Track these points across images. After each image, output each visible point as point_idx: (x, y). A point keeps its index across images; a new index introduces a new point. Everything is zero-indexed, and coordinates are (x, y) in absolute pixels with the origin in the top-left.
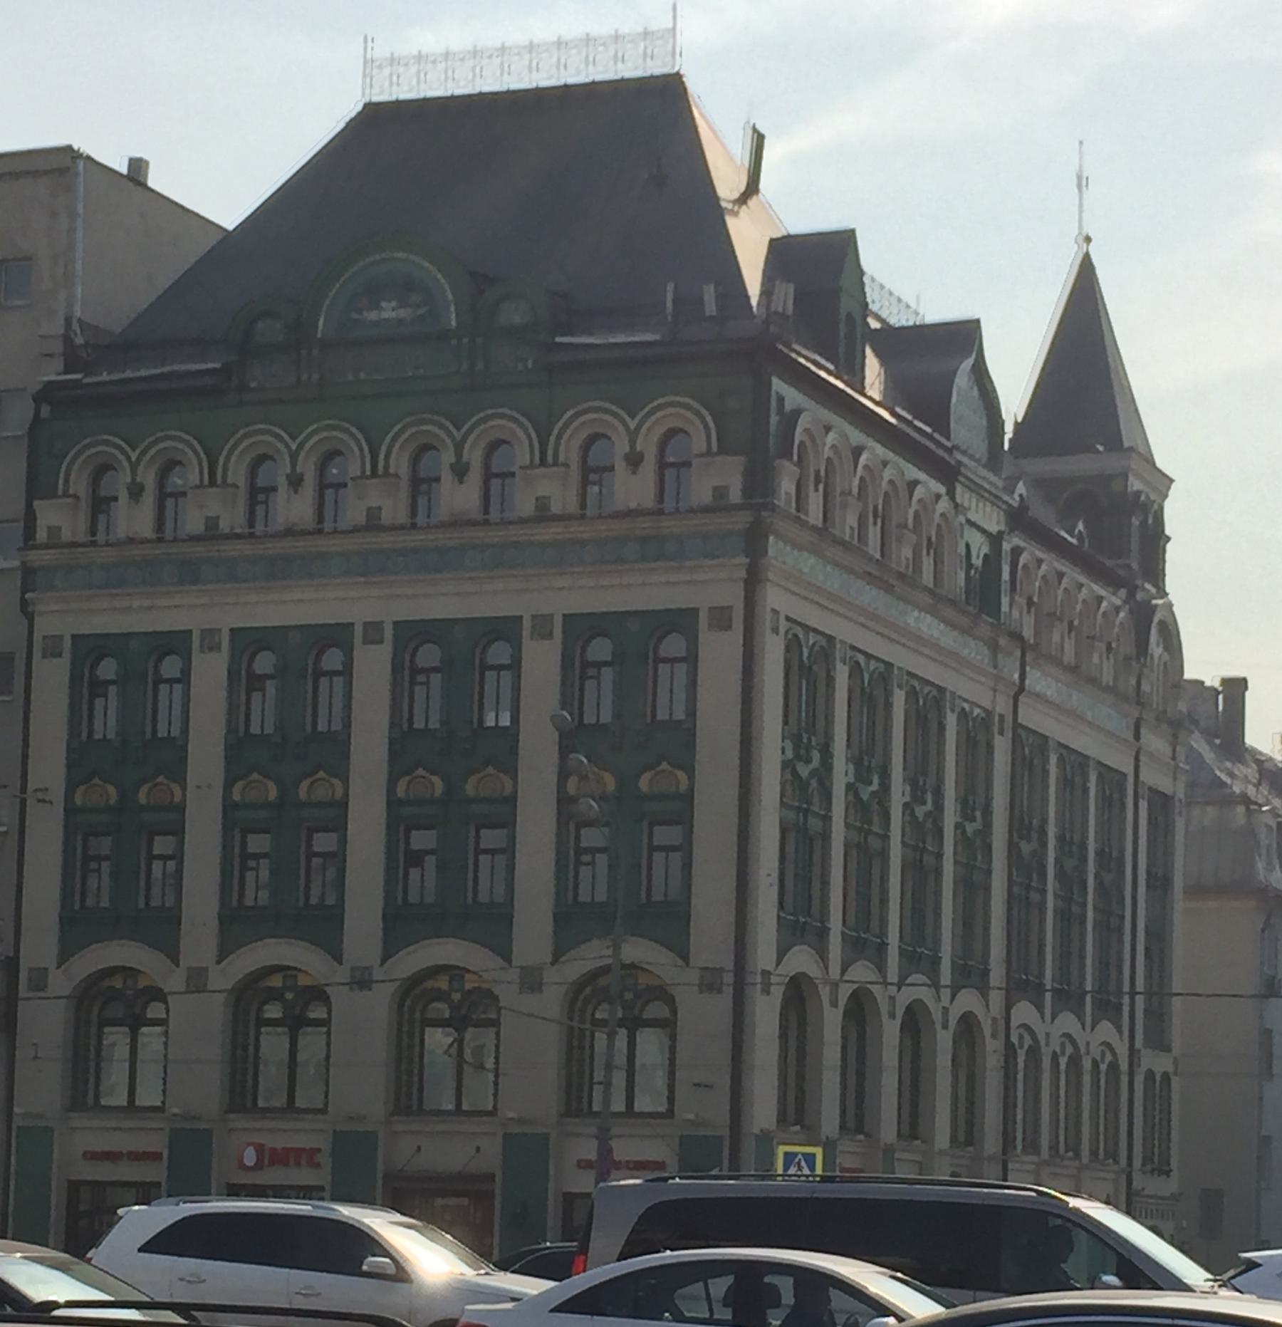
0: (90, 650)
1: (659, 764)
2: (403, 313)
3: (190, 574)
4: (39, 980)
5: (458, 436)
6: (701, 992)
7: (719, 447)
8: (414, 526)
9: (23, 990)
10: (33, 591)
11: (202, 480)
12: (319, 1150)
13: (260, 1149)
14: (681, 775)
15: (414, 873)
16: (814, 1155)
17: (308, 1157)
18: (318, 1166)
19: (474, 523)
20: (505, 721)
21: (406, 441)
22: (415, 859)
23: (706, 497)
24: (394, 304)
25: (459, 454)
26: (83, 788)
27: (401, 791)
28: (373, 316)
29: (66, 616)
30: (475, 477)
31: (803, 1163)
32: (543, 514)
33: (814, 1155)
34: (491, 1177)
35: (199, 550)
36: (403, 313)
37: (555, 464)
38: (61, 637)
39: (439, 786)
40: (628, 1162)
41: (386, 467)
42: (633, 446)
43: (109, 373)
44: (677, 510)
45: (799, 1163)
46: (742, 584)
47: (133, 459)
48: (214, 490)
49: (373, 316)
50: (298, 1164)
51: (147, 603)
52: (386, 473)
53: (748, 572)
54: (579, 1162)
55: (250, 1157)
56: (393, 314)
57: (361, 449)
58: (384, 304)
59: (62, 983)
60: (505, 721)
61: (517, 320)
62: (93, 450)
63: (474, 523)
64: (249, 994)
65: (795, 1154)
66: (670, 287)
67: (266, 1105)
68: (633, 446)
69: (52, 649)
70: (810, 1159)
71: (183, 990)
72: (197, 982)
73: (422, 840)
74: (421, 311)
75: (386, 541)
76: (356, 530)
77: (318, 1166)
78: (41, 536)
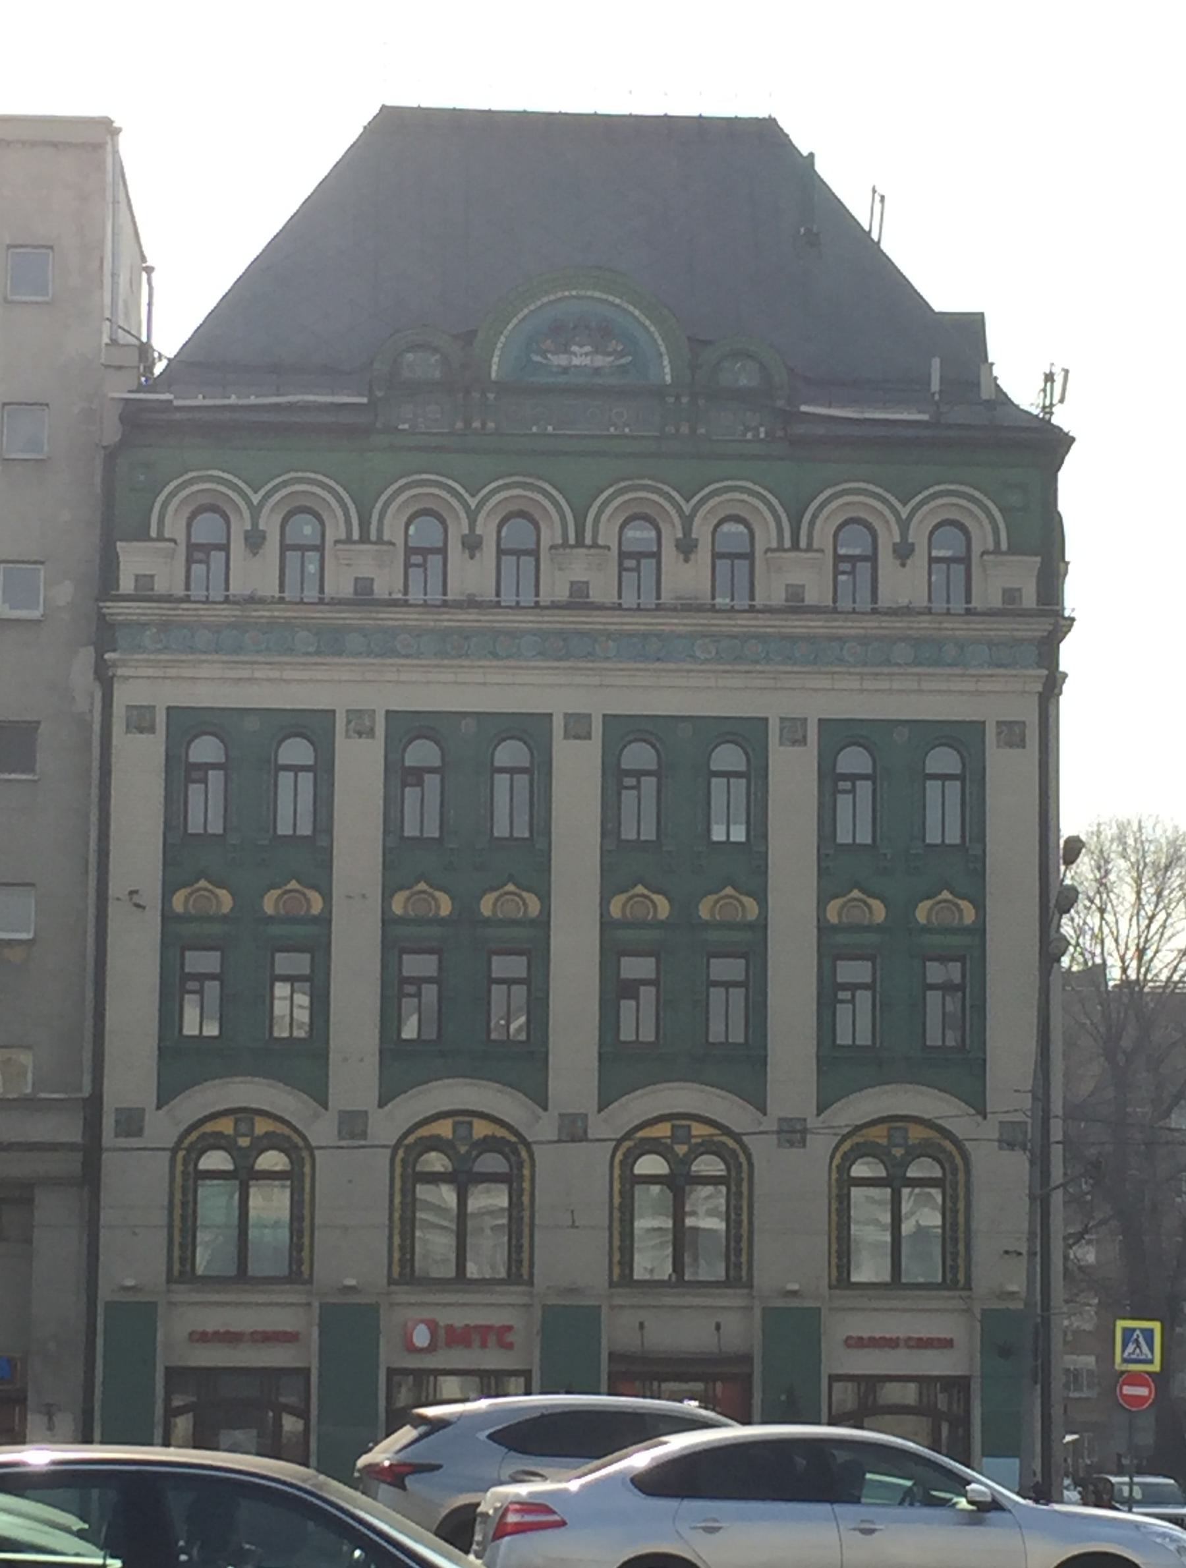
0: (186, 724)
1: (197, 880)
2: (600, 361)
3: (331, 642)
4: (131, 1123)
5: (687, 508)
6: (1001, 1148)
7: (361, 537)
8: (498, 605)
9: (108, 1136)
10: (114, 650)
11: (997, 543)
12: (509, 1328)
13: (433, 1326)
14: (748, 901)
15: (627, 1006)
16: (1151, 1331)
17: (500, 1336)
18: (510, 1346)
19: (700, 609)
20: (739, 834)
21: (617, 508)
22: (630, 989)
23: (562, 593)
24: (588, 349)
25: (687, 530)
26: (712, 898)
27: (397, 908)
28: (561, 360)
29: (148, 684)
30: (703, 555)
31: (1141, 1339)
32: (795, 605)
33: (1151, 1331)
34: (747, 1359)
35: (350, 617)
36: (600, 361)
37: (809, 548)
38: (152, 708)
39: (445, 906)
40: (910, 1339)
41: (380, 531)
42: (255, 524)
43: (238, 397)
44: (537, 605)
45: (1137, 1341)
46: (1036, 698)
47: (904, 516)
48: (582, 551)
49: (561, 360)
50: (484, 1345)
51: (275, 674)
52: (380, 541)
53: (1045, 685)
54: (849, 1338)
55: (421, 1337)
56: (587, 361)
57: (563, 517)
58: (575, 348)
59: (163, 1127)
60: (739, 834)
61: (743, 381)
62: (195, 488)
63: (700, 609)
64: (195, 1141)
65: (1134, 1330)
66: (936, 363)
67: (692, 1278)
68: (255, 524)
69: (141, 721)
70: (1148, 1334)
71: (556, 1138)
72: (353, 1126)
73: (636, 968)
74: (623, 361)
75: (597, 621)
76: (554, 606)
77: (510, 1346)
78: (126, 585)
